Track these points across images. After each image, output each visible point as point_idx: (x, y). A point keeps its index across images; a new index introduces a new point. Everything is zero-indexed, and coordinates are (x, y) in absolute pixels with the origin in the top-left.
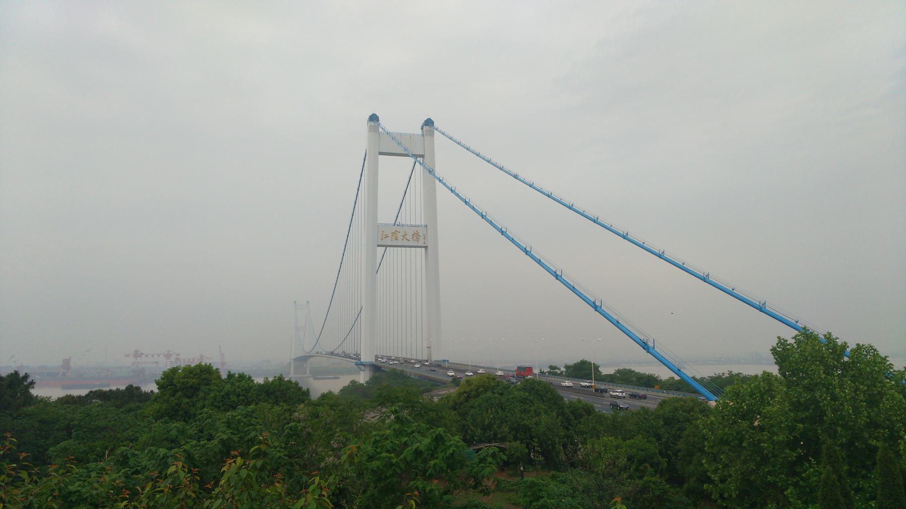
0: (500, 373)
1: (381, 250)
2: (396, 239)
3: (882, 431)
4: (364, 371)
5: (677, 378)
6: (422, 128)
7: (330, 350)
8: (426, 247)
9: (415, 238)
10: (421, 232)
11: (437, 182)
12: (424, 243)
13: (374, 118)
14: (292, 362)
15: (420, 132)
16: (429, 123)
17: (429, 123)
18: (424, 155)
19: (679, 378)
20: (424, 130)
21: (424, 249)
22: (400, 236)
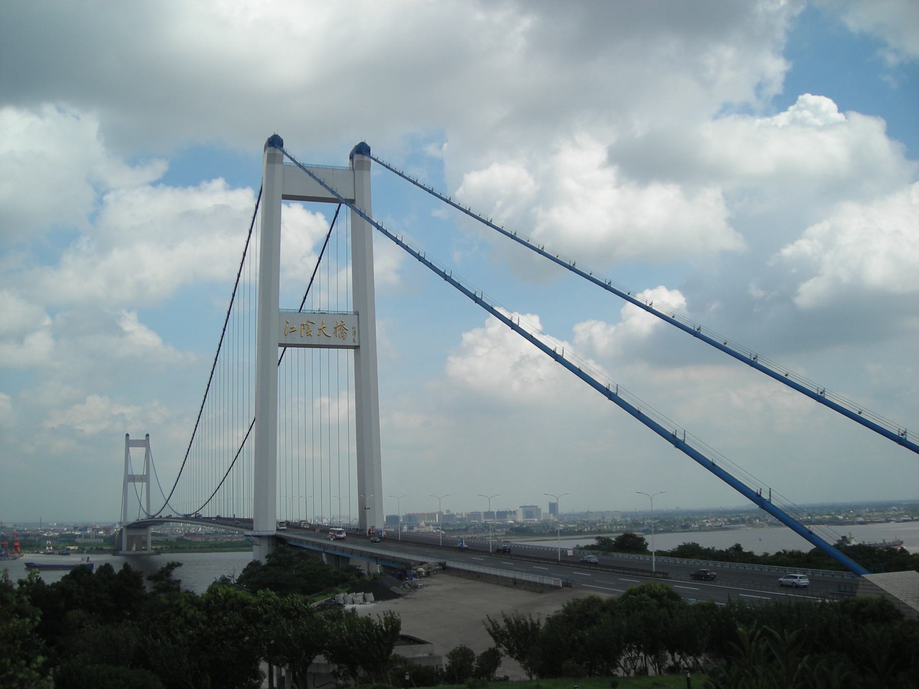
0: (794, 271)
1: (281, 349)
2: (309, 335)
3: (835, 601)
4: (260, 545)
5: (68, 572)
6: (351, 158)
7: (190, 510)
8: (356, 348)
9: (339, 333)
10: (350, 324)
11: (374, 229)
12: (354, 341)
13: (275, 142)
14: (124, 532)
15: (346, 163)
16: (362, 150)
17: (362, 150)
18: (355, 200)
19: (812, 547)
20: (355, 160)
21: (352, 351)
22: (315, 331)
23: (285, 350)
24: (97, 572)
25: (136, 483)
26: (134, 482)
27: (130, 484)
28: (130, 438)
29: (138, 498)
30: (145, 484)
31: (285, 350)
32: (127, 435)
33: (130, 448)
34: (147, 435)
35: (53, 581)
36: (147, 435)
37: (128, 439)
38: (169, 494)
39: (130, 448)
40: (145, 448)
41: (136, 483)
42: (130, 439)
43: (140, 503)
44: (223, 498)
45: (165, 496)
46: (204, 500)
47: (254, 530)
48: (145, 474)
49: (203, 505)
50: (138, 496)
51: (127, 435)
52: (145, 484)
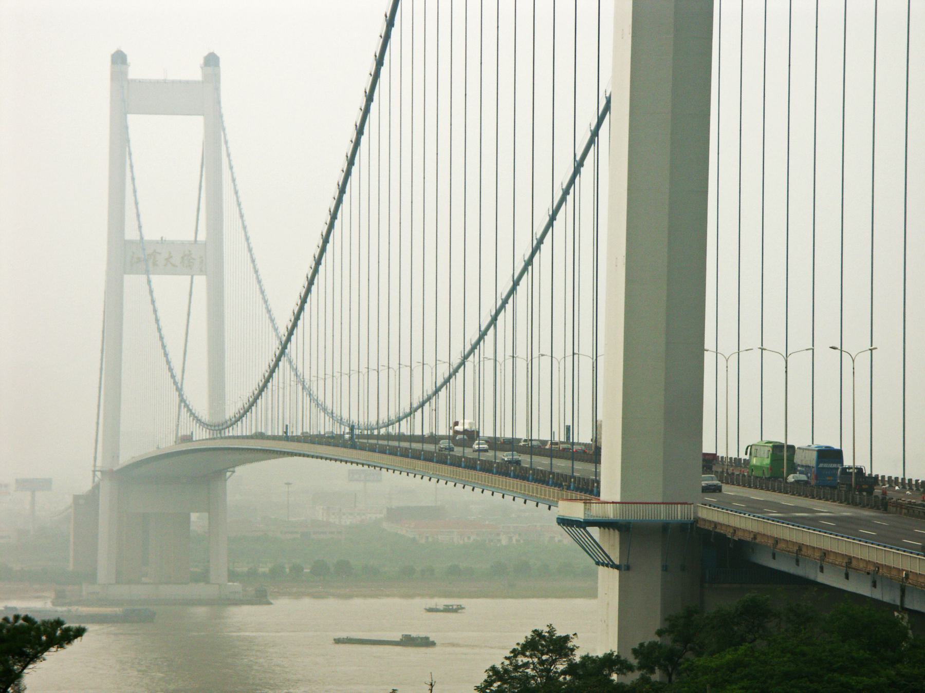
23: (400, 424)
24: (65, 628)
25: (155, 278)
26: (147, 272)
27: (134, 282)
28: (135, 72)
29: (173, 377)
30: (201, 281)
31: (400, 424)
32: (119, 59)
33: (129, 116)
34: (212, 61)
35: (72, 646)
36: (212, 61)
37: (125, 73)
38: (296, 300)
39: (129, 116)
40: (200, 119)
41: (155, 278)
42: (131, 76)
43: (179, 390)
44: (509, 352)
45: (275, 314)
46: (443, 355)
47: (603, 497)
48: (202, 237)
49: (440, 381)
50: (171, 369)
51: (119, 59)
52: (201, 281)
